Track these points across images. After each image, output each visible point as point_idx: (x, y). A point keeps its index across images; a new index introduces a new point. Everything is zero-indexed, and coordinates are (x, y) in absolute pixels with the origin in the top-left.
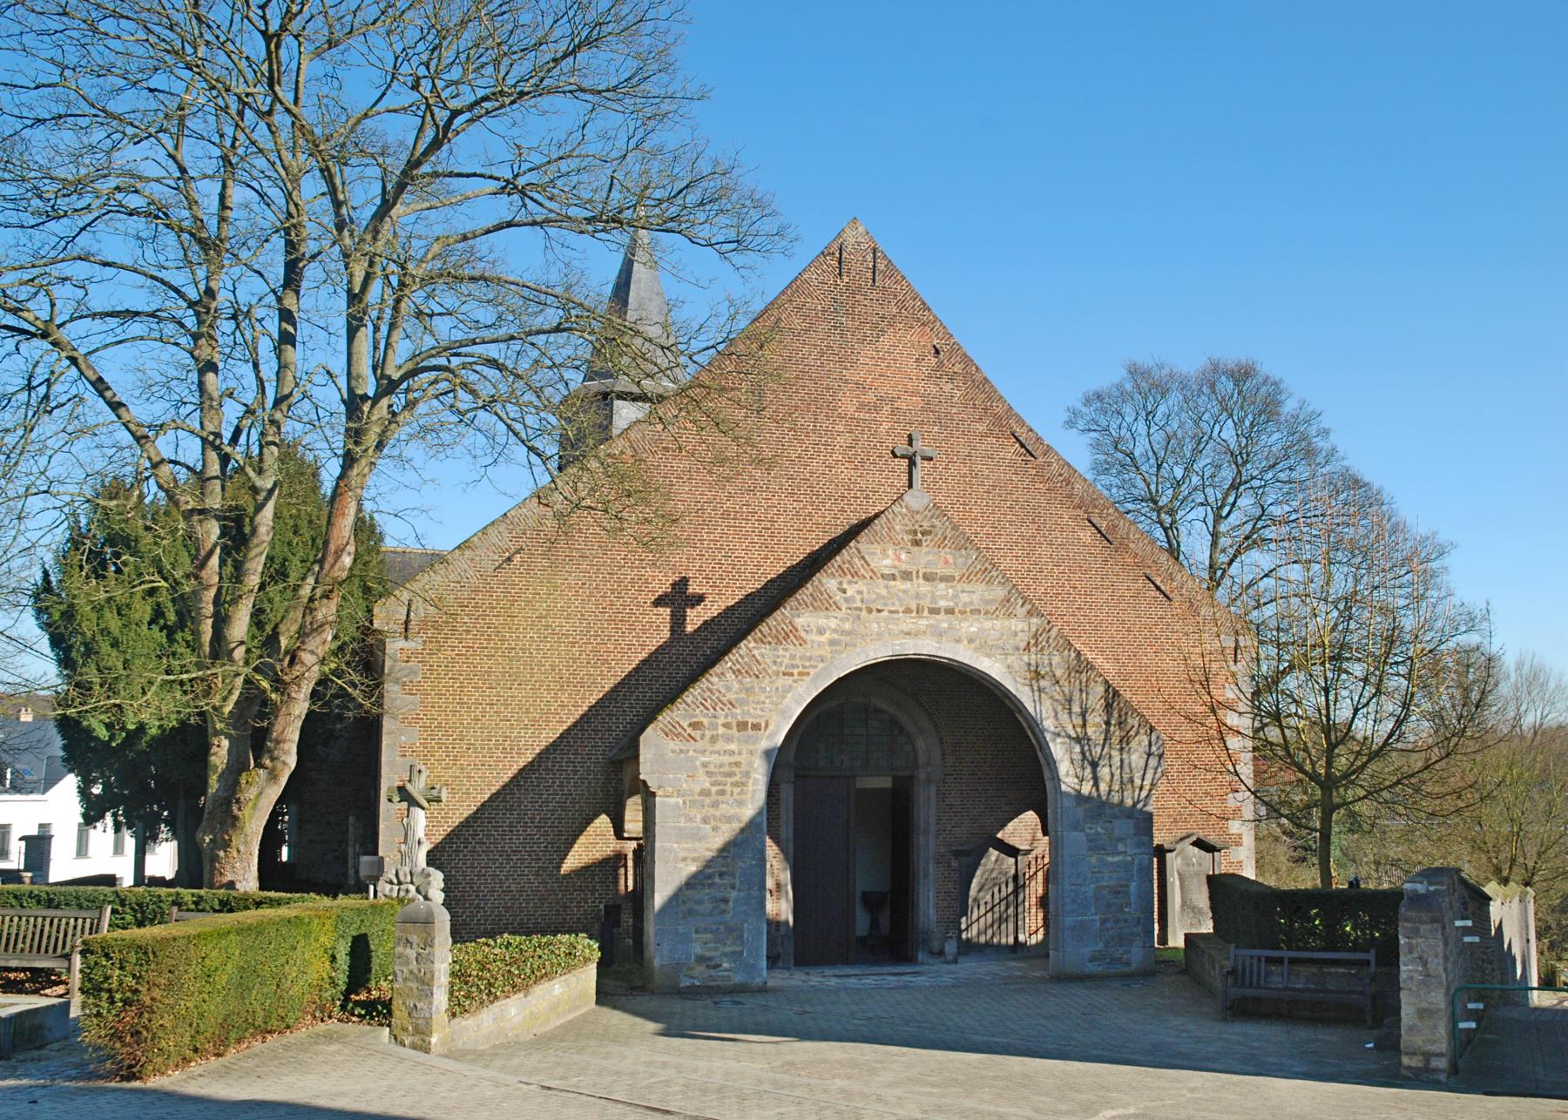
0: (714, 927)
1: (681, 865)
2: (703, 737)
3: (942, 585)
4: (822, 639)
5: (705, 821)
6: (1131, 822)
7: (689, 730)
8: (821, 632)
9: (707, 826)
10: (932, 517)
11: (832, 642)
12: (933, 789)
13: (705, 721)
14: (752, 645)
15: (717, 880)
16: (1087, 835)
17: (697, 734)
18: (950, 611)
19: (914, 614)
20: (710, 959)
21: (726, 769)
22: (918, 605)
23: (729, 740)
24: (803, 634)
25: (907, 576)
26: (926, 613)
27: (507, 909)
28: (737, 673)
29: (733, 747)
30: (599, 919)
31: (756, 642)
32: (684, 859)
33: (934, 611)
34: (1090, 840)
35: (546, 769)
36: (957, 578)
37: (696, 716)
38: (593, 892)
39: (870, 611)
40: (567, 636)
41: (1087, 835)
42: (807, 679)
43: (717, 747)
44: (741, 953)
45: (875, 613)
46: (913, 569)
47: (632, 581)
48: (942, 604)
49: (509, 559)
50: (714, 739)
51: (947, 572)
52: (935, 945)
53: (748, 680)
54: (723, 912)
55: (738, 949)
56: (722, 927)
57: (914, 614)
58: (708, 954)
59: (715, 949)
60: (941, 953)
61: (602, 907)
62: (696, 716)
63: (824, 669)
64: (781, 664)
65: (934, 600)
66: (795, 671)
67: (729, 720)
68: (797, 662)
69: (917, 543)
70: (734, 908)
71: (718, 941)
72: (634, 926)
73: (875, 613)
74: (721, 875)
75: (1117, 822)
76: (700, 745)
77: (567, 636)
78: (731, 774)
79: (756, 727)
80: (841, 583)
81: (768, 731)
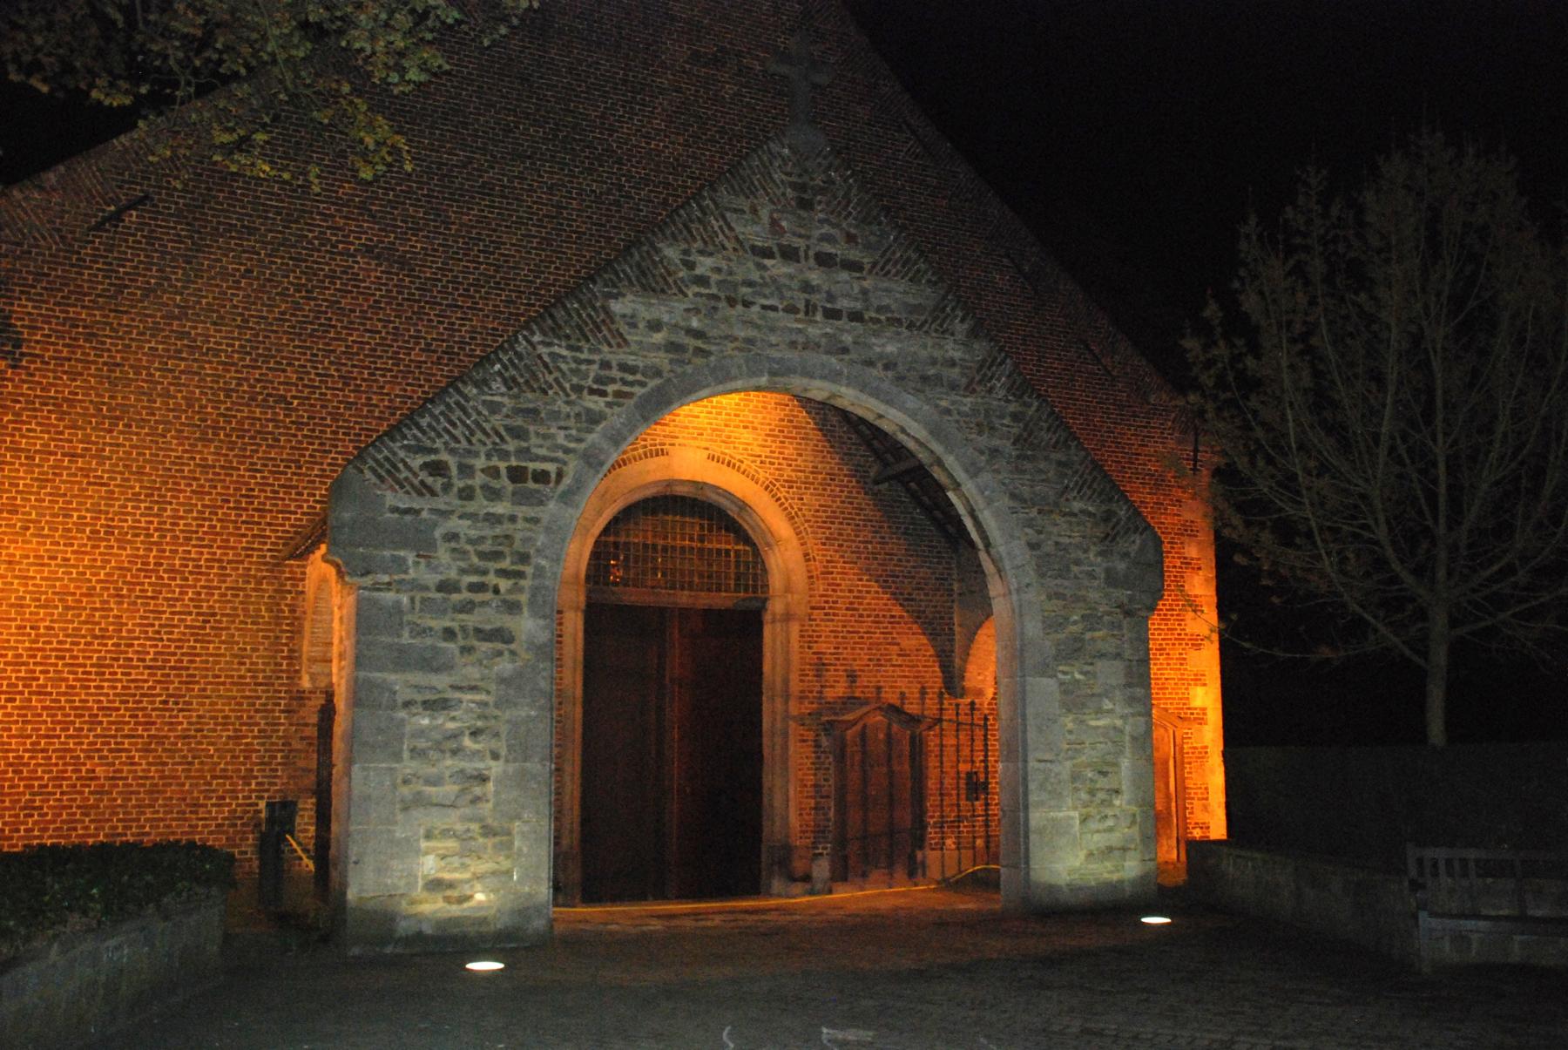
0: (459, 827)
1: (402, 714)
2: (447, 488)
3: (844, 275)
4: (658, 337)
5: (449, 634)
6: (1119, 665)
7: (423, 475)
8: (655, 326)
9: (451, 645)
10: (829, 167)
11: (672, 347)
12: (795, 628)
13: (452, 461)
14: (537, 338)
15: (467, 742)
16: (1062, 684)
17: (437, 483)
18: (856, 316)
19: (801, 316)
20: (451, 885)
21: (486, 547)
22: (807, 302)
23: (494, 494)
24: (624, 329)
25: (789, 254)
26: (819, 317)
27: (86, 809)
28: (510, 383)
29: (500, 508)
30: (258, 825)
31: (544, 334)
32: (407, 704)
33: (833, 314)
34: (1065, 692)
35: (171, 570)
36: (867, 267)
37: (436, 451)
38: (246, 780)
39: (732, 302)
40: (217, 353)
41: (1062, 684)
42: (631, 402)
43: (471, 507)
44: (509, 873)
45: (740, 307)
46: (799, 243)
47: (332, 277)
48: (843, 304)
49: (117, 217)
50: (467, 494)
51: (854, 254)
52: (798, 865)
53: (530, 395)
54: (476, 800)
55: (506, 864)
56: (475, 827)
57: (801, 316)
58: (447, 876)
59: (464, 866)
60: (807, 878)
61: (262, 805)
62: (436, 451)
63: (659, 389)
64: (586, 377)
65: (831, 297)
66: (610, 388)
67: (495, 462)
68: (615, 373)
69: (806, 205)
70: (497, 793)
71: (466, 852)
72: (317, 837)
73: (740, 307)
74: (475, 734)
75: (1100, 665)
76: (440, 503)
77: (217, 353)
78: (497, 556)
79: (541, 477)
80: (686, 252)
81: (562, 487)
